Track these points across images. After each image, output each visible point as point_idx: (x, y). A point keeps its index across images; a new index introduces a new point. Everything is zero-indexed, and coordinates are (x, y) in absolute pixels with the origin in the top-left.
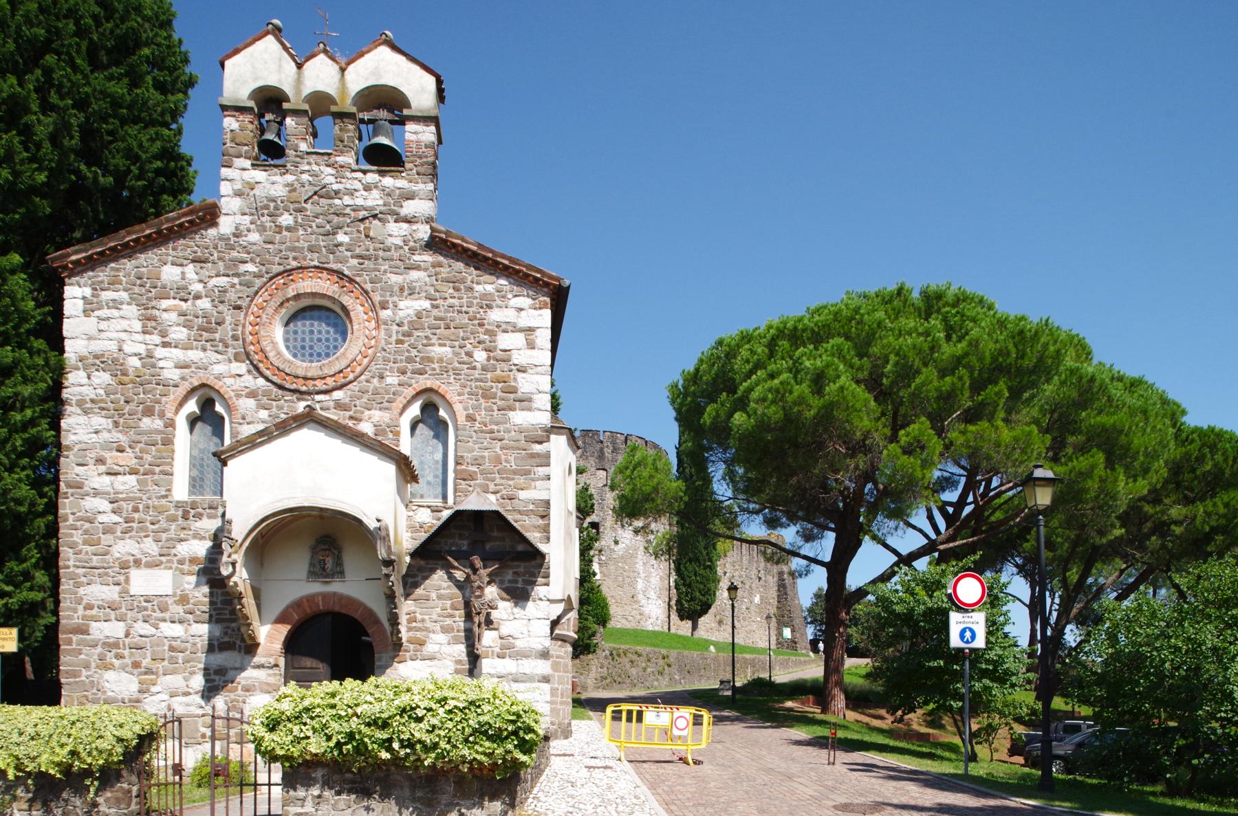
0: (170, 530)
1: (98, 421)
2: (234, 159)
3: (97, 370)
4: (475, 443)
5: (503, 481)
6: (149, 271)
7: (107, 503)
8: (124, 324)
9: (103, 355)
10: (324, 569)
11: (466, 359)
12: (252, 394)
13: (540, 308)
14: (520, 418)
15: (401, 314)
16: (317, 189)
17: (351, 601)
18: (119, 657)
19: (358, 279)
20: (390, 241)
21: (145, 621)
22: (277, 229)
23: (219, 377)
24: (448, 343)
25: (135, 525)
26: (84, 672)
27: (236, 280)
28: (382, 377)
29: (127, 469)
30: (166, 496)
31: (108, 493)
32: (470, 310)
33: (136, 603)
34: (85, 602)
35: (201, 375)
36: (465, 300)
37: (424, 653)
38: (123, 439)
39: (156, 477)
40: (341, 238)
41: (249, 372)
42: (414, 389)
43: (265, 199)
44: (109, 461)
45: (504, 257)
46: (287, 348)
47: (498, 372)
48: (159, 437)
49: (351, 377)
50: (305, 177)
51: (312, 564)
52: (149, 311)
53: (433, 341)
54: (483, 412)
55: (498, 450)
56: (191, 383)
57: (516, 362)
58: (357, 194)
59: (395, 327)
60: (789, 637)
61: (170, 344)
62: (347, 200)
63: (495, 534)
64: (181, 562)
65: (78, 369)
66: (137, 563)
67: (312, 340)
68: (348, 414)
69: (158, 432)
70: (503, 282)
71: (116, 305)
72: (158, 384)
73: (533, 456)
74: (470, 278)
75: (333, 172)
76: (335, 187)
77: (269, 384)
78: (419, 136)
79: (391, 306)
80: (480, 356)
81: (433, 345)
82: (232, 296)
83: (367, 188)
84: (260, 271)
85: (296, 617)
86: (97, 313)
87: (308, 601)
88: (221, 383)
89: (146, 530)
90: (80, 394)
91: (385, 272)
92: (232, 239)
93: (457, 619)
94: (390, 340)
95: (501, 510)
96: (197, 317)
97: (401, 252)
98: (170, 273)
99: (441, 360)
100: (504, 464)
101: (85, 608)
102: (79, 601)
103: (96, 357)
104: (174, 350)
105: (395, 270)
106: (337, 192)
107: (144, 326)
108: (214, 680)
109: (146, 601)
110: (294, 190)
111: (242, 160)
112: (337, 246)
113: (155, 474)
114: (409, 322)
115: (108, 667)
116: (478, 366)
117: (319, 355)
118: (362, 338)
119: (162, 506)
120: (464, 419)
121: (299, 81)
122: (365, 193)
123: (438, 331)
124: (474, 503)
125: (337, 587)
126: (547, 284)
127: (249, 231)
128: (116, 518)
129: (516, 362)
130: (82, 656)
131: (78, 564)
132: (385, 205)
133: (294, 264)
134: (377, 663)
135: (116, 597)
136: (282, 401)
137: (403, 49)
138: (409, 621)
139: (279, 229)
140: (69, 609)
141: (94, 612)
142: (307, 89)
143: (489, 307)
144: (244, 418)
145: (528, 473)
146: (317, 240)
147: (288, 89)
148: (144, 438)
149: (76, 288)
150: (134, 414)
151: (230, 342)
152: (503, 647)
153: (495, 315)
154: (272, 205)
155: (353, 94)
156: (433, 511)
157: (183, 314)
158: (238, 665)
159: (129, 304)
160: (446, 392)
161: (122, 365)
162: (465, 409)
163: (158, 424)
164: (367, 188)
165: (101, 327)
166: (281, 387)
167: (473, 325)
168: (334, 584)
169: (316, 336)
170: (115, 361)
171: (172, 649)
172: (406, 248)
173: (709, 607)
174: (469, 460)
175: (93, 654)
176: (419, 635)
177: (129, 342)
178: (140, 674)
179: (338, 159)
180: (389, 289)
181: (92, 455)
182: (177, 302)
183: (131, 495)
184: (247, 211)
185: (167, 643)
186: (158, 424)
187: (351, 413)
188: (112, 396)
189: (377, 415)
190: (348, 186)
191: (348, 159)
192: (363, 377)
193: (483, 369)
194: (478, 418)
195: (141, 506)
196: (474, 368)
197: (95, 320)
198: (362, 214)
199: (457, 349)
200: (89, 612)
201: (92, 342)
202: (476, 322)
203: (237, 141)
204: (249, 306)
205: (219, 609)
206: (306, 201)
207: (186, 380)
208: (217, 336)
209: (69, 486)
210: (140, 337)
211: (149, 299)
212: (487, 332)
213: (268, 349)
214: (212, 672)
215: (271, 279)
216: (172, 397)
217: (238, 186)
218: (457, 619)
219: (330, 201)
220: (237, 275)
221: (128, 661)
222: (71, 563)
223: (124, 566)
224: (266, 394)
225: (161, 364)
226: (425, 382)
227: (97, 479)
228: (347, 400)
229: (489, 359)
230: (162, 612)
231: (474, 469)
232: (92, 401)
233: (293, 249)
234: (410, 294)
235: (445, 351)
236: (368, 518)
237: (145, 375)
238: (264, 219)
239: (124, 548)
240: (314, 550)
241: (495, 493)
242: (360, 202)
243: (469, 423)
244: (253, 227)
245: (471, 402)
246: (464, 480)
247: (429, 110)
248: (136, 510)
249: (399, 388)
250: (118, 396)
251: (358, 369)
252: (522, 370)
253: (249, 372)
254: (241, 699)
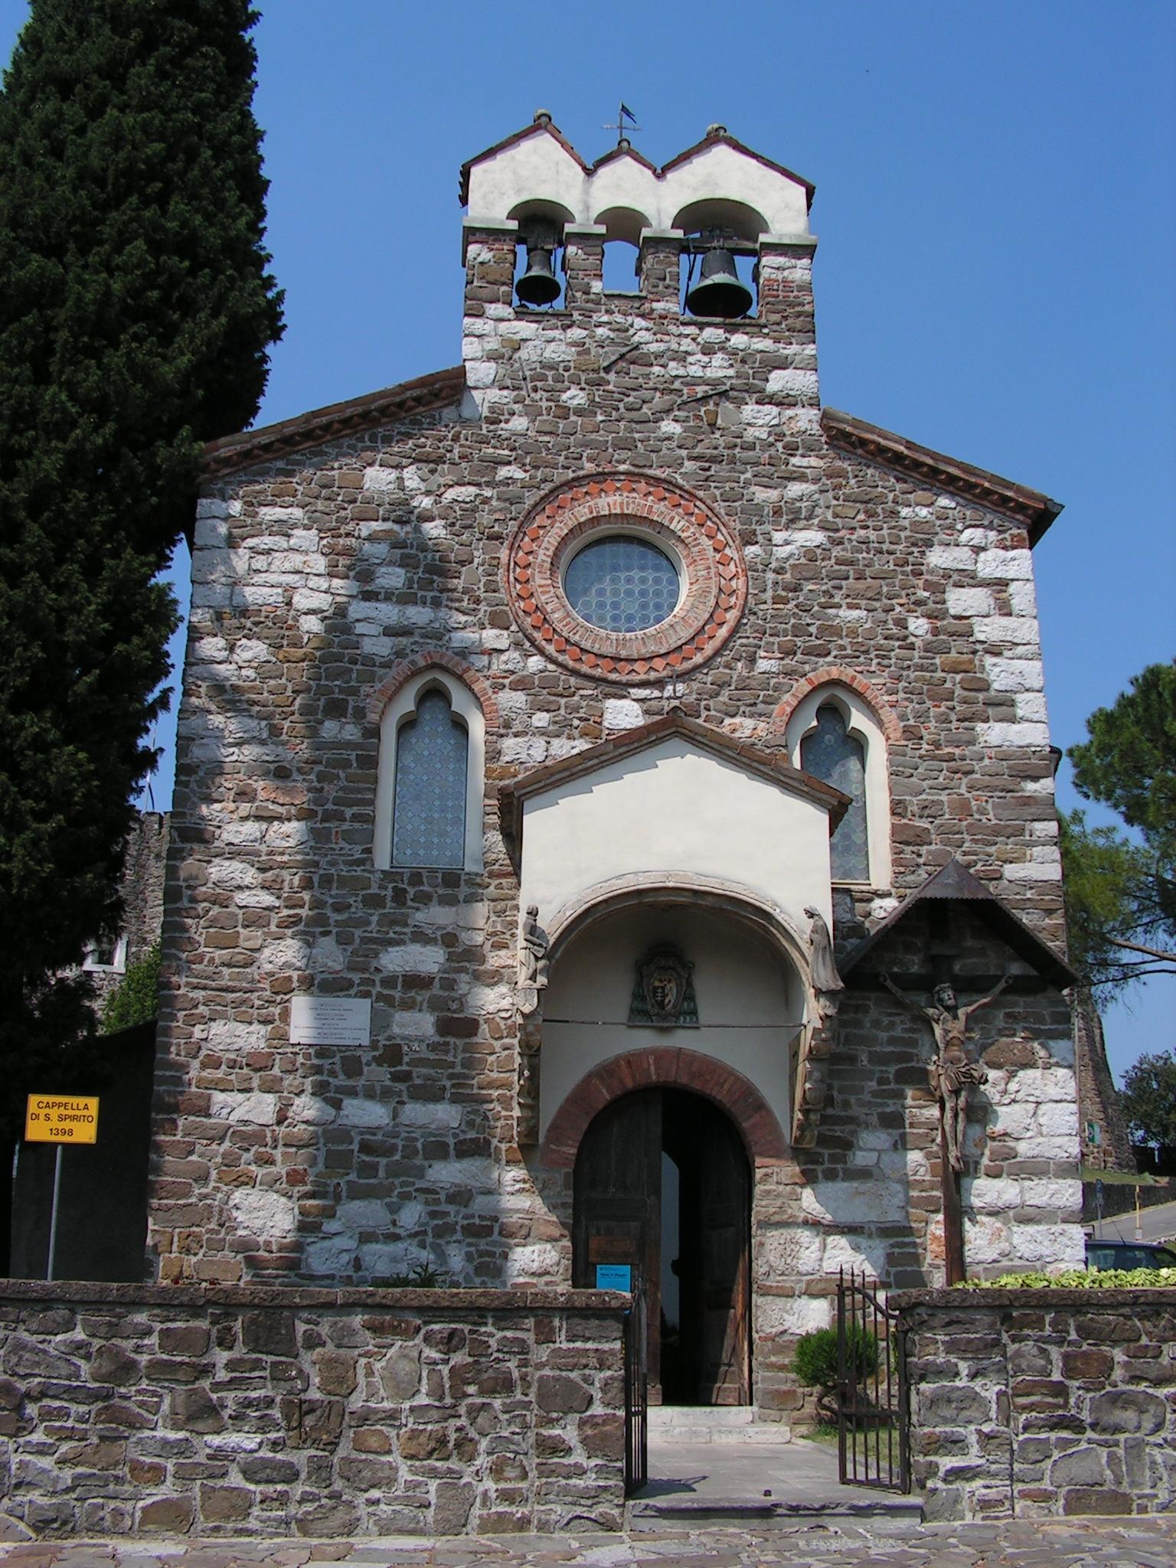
0: (369, 923)
2: (486, 305)
5: (976, 847)
6: (342, 476)
8: (297, 560)
10: (661, 1005)
13: (1014, 548)
17: (710, 1067)
19: (701, 494)
20: (751, 434)
22: (559, 412)
27: (488, 492)
28: (752, 660)
29: (293, 811)
30: (360, 862)
35: (431, 648)
36: (885, 532)
39: (346, 826)
43: (538, 365)
45: (950, 461)
47: (953, 654)
51: (638, 996)
53: (836, 600)
57: (982, 637)
58: (690, 359)
59: (770, 576)
67: (615, 592)
69: (349, 745)
70: (944, 501)
71: (284, 529)
74: (891, 496)
76: (654, 347)
80: (918, 626)
81: (839, 606)
82: (485, 518)
83: (708, 350)
86: (251, 542)
87: (629, 1063)
91: (747, 483)
94: (764, 596)
97: (773, 451)
99: (853, 633)
100: (977, 816)
104: (382, 606)
113: (345, 820)
114: (793, 566)
115: (246, 1181)
116: (918, 643)
120: (899, 735)
125: (683, 1040)
126: (1021, 508)
128: (268, 899)
130: (194, 1158)
132: (738, 377)
133: (589, 467)
136: (576, 698)
139: (564, 412)
153: (938, 558)
154: (550, 374)
157: (397, 544)
159: (307, 528)
161: (289, 628)
162: (903, 717)
163: (351, 732)
164: (708, 350)
165: (256, 565)
166: (575, 673)
167: (903, 573)
168: (680, 1033)
170: (280, 622)
172: (780, 445)
174: (915, 809)
179: (655, 305)
180: (756, 511)
182: (388, 525)
184: (509, 382)
185: (357, 1139)
186: (351, 732)
188: (272, 682)
191: (673, 306)
196: (911, 647)
198: (700, 390)
199: (882, 616)
203: (490, 278)
210: (323, 583)
211: (343, 521)
217: (493, 344)
219: (647, 370)
224: (548, 684)
225: (360, 628)
226: (826, 669)
229: (935, 632)
231: (924, 824)
234: (792, 521)
242: (695, 371)
244: (517, 407)
246: (908, 844)
247: (799, 236)
254: (498, 1251)
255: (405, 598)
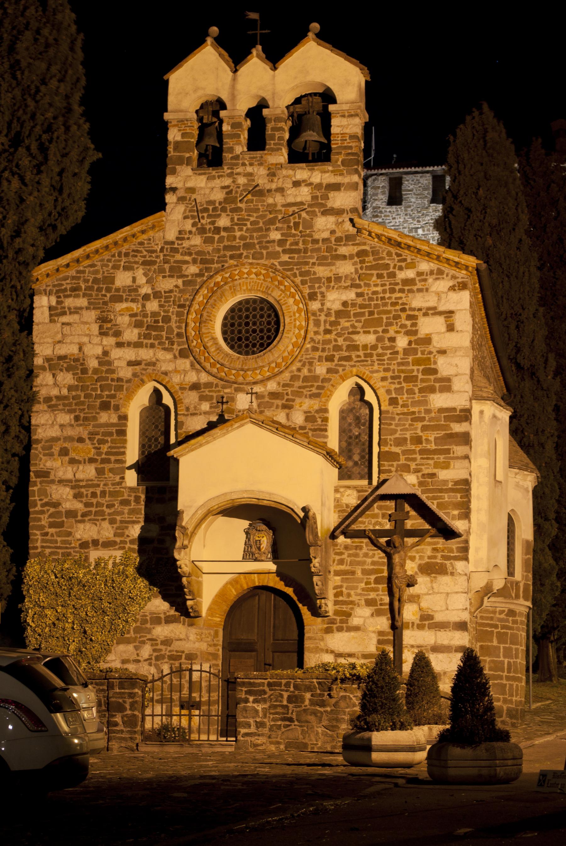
1: (65, 418)
12: (195, 387)
37: (349, 624)
46: (225, 340)
53: (358, 330)
61: (124, 343)
69: (113, 425)
71: (76, 311)
73: (452, 436)
81: (358, 333)
83: (297, 184)
85: (235, 593)
89: (102, 513)
93: (380, 593)
95: (419, 493)
99: (365, 347)
105: (323, 260)
106: (269, 191)
107: (101, 327)
108: (160, 650)
112: (268, 242)
116: (401, 350)
117: (254, 345)
120: (387, 403)
131: (44, 544)
138: (336, 595)
139: (217, 230)
145: (448, 451)
158: (182, 636)
159: (87, 308)
164: (297, 184)
167: (396, 311)
169: (251, 327)
183: (90, 483)
186: (114, 419)
193: (405, 354)
202: (398, 307)
209: (37, 476)
212: (409, 317)
213: (209, 345)
214: (159, 642)
218: (380, 593)
222: (39, 544)
235: (371, 339)
238: (203, 221)
248: (94, 495)
252: (443, 352)
255: (137, 345)
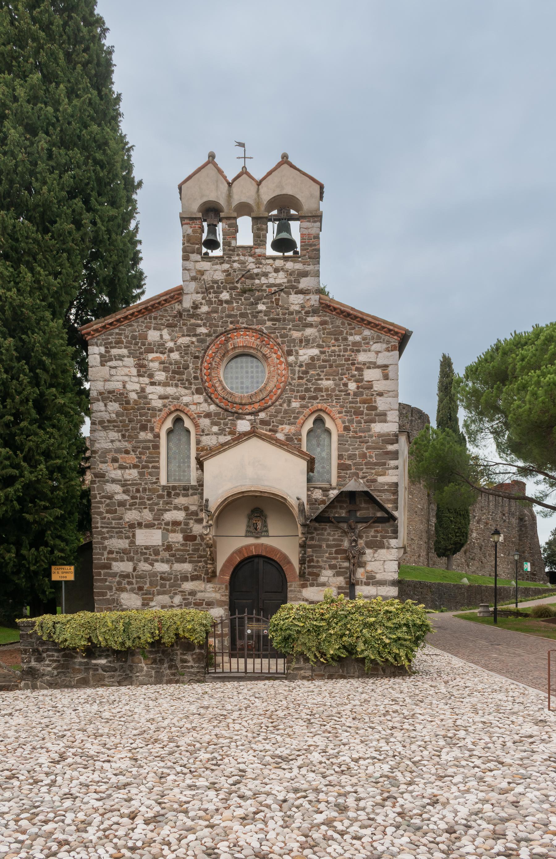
1: (114, 435)
2: (190, 255)
3: (111, 401)
4: (350, 445)
5: (368, 471)
7: (119, 487)
8: (126, 370)
9: (114, 392)
10: (256, 529)
11: (343, 388)
12: (208, 415)
13: (392, 350)
14: (378, 428)
15: (301, 359)
16: (244, 273)
18: (130, 583)
21: (145, 561)
23: (187, 405)
24: (331, 377)
25: (137, 501)
26: (109, 594)
27: (194, 339)
28: (289, 402)
30: (156, 483)
31: (120, 481)
32: (346, 354)
33: (139, 550)
34: (108, 549)
36: (342, 347)
38: (127, 445)
39: (150, 470)
40: (261, 307)
41: (206, 401)
42: (310, 410)
44: (120, 460)
47: (365, 396)
48: (151, 444)
49: (270, 403)
50: (236, 265)
51: (248, 526)
52: (141, 362)
54: (355, 425)
55: (364, 450)
56: (169, 409)
59: (297, 368)
60: (529, 570)
62: (264, 280)
63: (363, 505)
64: (167, 524)
65: (99, 401)
66: (140, 525)
68: (269, 427)
69: (149, 441)
71: (120, 358)
72: (149, 409)
73: (388, 453)
75: (254, 260)
76: (256, 271)
77: (218, 408)
78: (310, 230)
79: (294, 353)
80: (352, 386)
81: (322, 379)
83: (277, 270)
84: (210, 332)
88: (188, 409)
89: (144, 504)
90: (101, 417)
91: (290, 329)
92: (191, 310)
96: (171, 364)
98: (153, 336)
99: (327, 390)
101: (108, 553)
102: (105, 548)
103: (110, 392)
105: (296, 328)
106: (257, 275)
107: (138, 371)
109: (145, 549)
110: (229, 275)
111: (195, 255)
116: (352, 393)
118: (276, 376)
119: (154, 489)
120: (342, 429)
121: (229, 196)
122: (275, 275)
123: (325, 370)
124: (352, 486)
125: (263, 541)
127: (201, 304)
128: (126, 497)
129: (376, 389)
130: (107, 583)
133: (231, 326)
134: (289, 589)
135: (127, 546)
137: (298, 167)
139: (221, 302)
140: (98, 554)
141: (114, 556)
142: (235, 203)
143: (358, 351)
144: (203, 431)
146: (245, 309)
147: (222, 202)
148: (142, 445)
149: (95, 347)
150: (135, 430)
151: (193, 381)
152: (368, 578)
153: (362, 357)
154: (215, 286)
155: (265, 203)
156: (323, 491)
157: (162, 363)
159: (128, 357)
160: (331, 411)
161: (126, 397)
162: (344, 422)
163: (150, 436)
164: (277, 270)
166: (226, 410)
167: (348, 364)
170: (121, 394)
171: (162, 578)
173: (462, 545)
175: (114, 582)
176: (315, 570)
177: (129, 383)
178: (143, 594)
181: (109, 457)
182: (158, 355)
185: (159, 575)
186: (150, 436)
187: (271, 427)
188: (121, 418)
189: (287, 428)
190: (264, 270)
192: (277, 403)
194: (352, 428)
195: (141, 489)
196: (349, 394)
197: (108, 368)
198: (273, 289)
200: (110, 556)
201: (107, 383)
202: (350, 362)
204: (204, 356)
205: (190, 554)
206: (237, 282)
207: (166, 407)
208: (185, 377)
210: (136, 379)
211: (141, 353)
212: (357, 369)
213: (217, 385)
215: (217, 337)
216: (158, 418)
217: (193, 274)
220: (196, 335)
221: (135, 586)
222: (99, 525)
223: (132, 526)
224: (217, 414)
227: (114, 472)
228: (268, 418)
229: (358, 388)
230: (156, 555)
231: (349, 462)
232: (109, 421)
233: (229, 316)
236: (290, 497)
237: (140, 404)
238: (211, 296)
239: (131, 516)
240: (250, 518)
241: (363, 478)
242: (271, 281)
243: (345, 432)
244: (204, 301)
245: (347, 418)
248: (138, 491)
249: (301, 410)
250: (124, 418)
251: (274, 398)
252: (380, 394)
253: (206, 401)
